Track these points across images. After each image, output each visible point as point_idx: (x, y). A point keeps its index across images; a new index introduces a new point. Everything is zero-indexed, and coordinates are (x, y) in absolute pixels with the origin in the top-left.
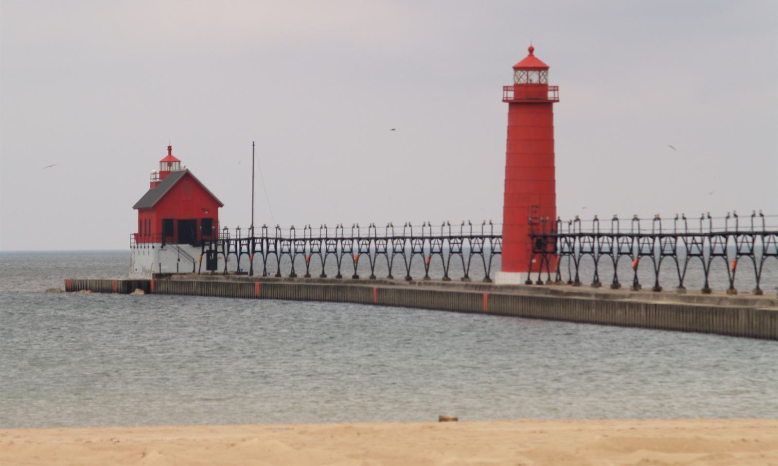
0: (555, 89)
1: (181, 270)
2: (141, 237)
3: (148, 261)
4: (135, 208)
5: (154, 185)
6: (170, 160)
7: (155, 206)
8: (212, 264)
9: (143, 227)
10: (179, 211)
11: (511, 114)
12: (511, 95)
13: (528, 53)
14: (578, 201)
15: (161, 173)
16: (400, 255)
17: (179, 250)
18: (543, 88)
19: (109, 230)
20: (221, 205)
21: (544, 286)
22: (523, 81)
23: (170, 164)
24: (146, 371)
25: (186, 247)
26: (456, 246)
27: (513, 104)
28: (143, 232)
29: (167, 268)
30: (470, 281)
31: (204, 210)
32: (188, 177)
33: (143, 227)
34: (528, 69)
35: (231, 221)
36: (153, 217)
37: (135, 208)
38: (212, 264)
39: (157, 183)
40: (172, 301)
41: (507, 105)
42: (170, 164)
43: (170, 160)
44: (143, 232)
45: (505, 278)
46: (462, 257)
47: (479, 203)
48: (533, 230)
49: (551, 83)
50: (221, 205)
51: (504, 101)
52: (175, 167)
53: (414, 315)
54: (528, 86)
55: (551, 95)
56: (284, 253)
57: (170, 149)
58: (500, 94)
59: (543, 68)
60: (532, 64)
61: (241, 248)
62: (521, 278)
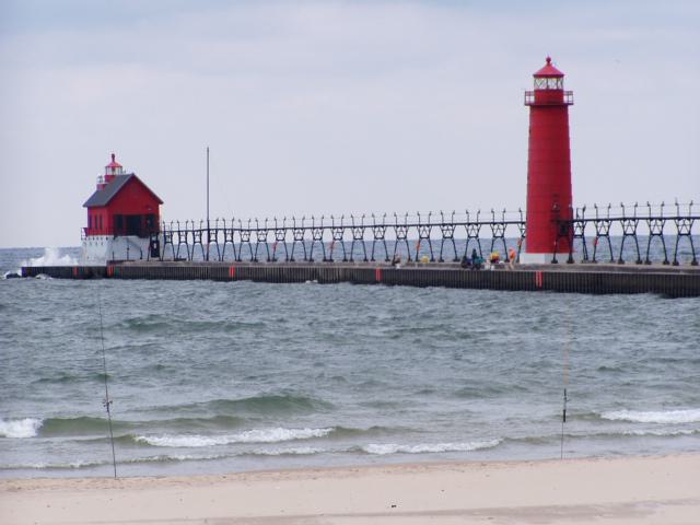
0: (570, 93)
1: (131, 257)
2: (90, 231)
3: (100, 251)
4: (84, 206)
5: (102, 188)
6: (113, 166)
7: (108, 205)
8: (155, 252)
9: (93, 221)
10: (125, 207)
11: (532, 116)
12: (532, 99)
13: (545, 63)
14: (588, 193)
15: (107, 177)
16: (686, 238)
17: (128, 241)
18: (559, 93)
19: (59, 229)
20: (161, 203)
21: (616, 265)
22: (543, 87)
23: (113, 169)
24: (108, 345)
25: (133, 238)
27: (533, 107)
28: (93, 225)
29: (118, 257)
31: (148, 207)
32: (133, 179)
33: (93, 221)
34: (547, 76)
35: (167, 216)
36: (105, 214)
37: (84, 206)
38: (155, 252)
39: (104, 186)
41: (528, 107)
42: (113, 169)
43: (113, 166)
44: (93, 225)
45: (529, 259)
47: (497, 195)
48: (552, 214)
49: (566, 89)
50: (161, 203)
51: (526, 105)
52: (117, 172)
53: (673, 308)
54: (548, 91)
55: (565, 99)
57: (113, 156)
58: (521, 99)
59: (559, 76)
60: (550, 72)
62: (546, 259)
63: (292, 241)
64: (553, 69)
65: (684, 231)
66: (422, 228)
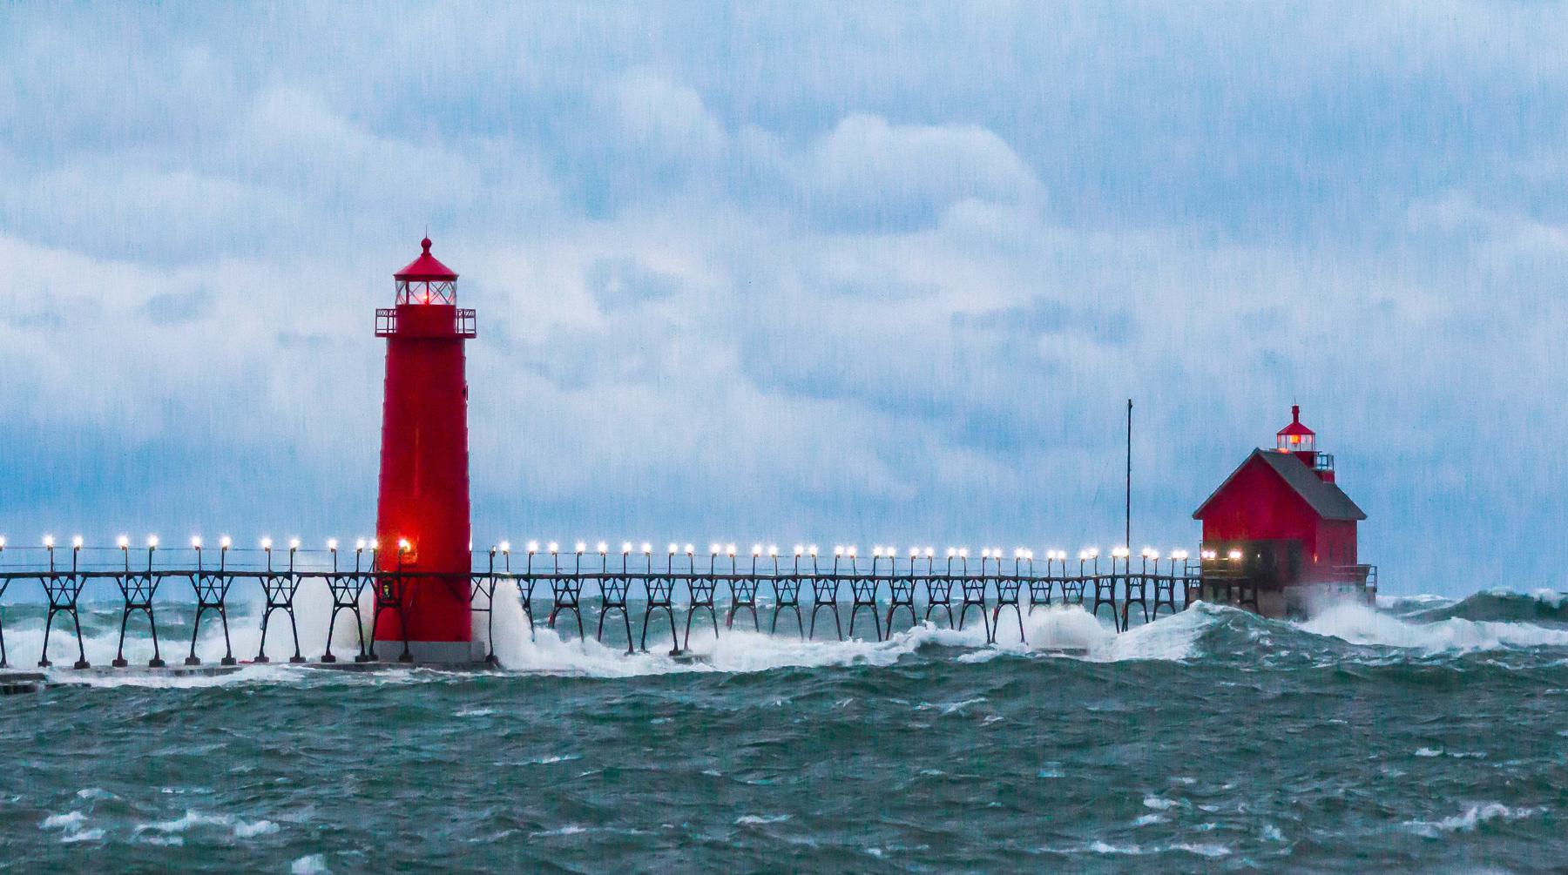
0: (472, 314)
4: (1197, 516)
13: (421, 250)
16: (746, 609)
20: (1364, 517)
26: (1073, 593)
30: (500, 667)
37: (1197, 516)
40: (760, 691)
46: (357, 613)
50: (1364, 517)
51: (378, 335)
56: (784, 604)
57: (1296, 410)
59: (449, 277)
60: (427, 269)
61: (1157, 595)
63: (888, 601)
64: (434, 263)
65: (211, 599)
66: (781, 585)
